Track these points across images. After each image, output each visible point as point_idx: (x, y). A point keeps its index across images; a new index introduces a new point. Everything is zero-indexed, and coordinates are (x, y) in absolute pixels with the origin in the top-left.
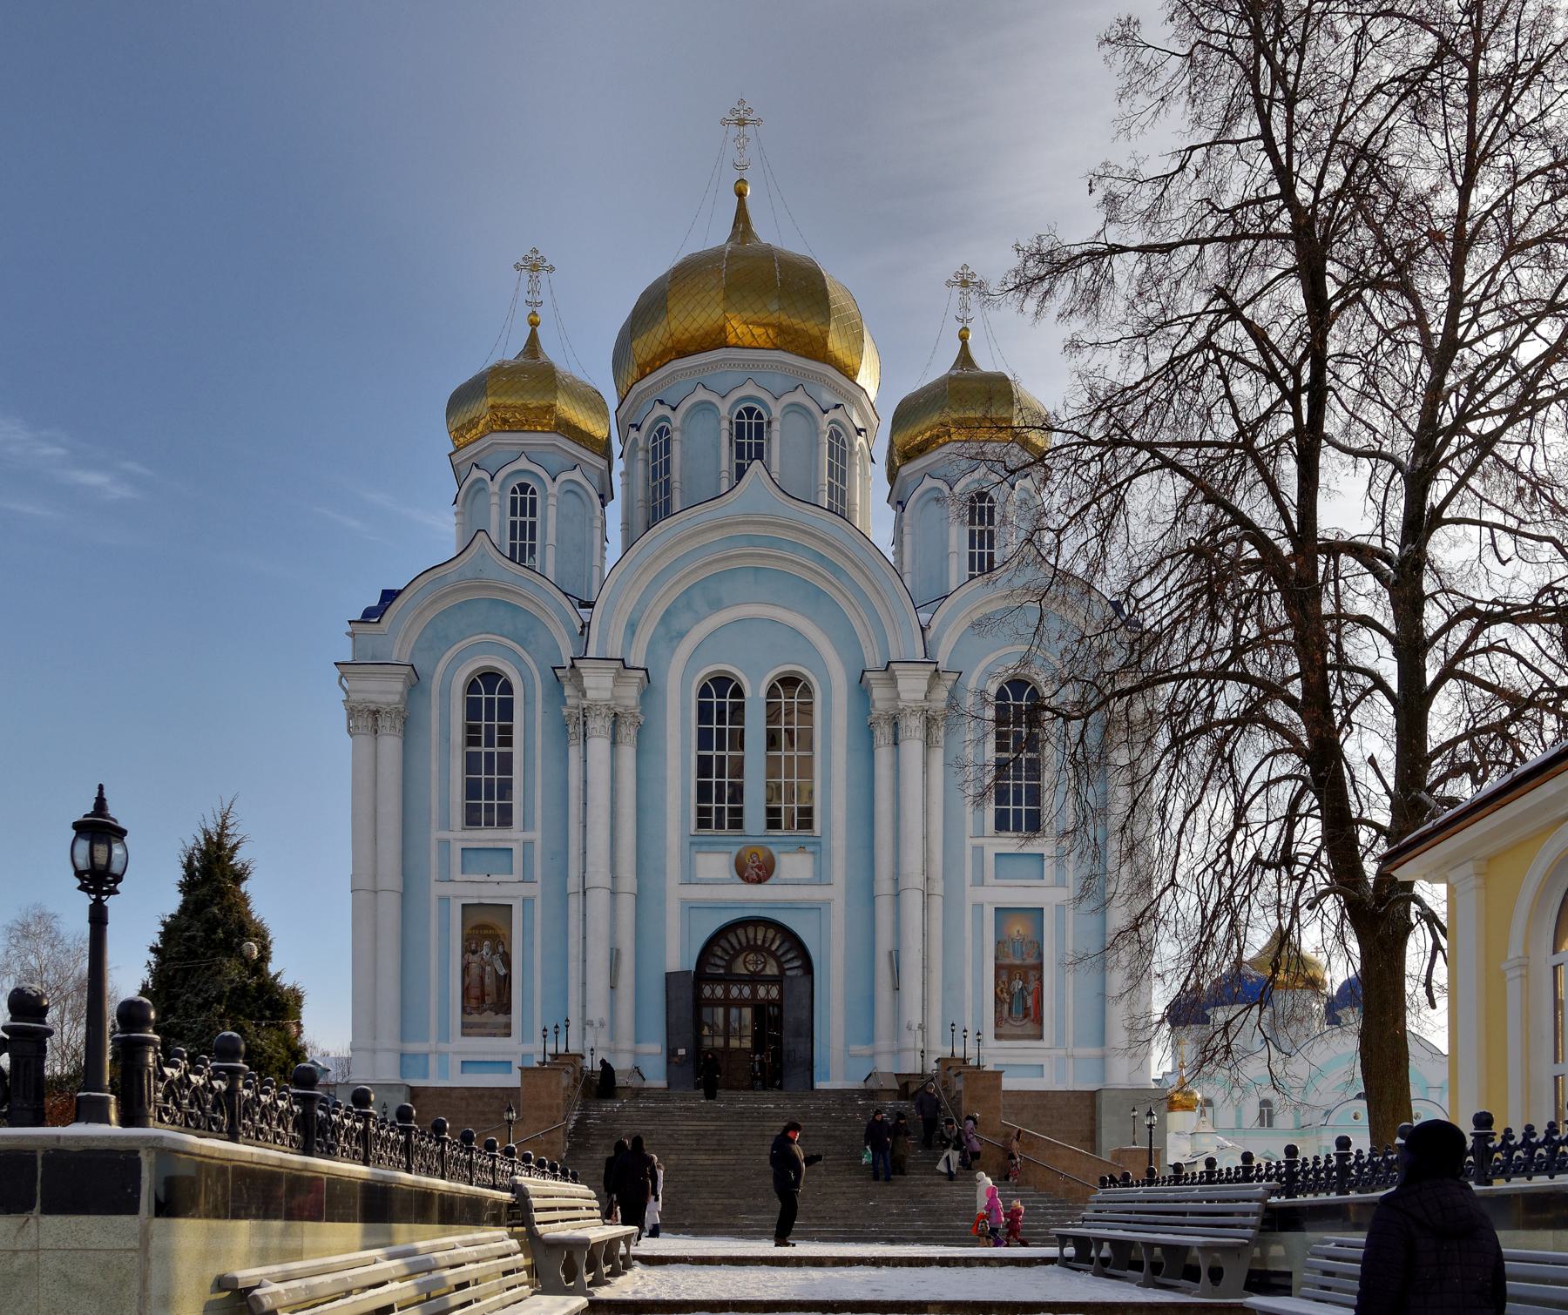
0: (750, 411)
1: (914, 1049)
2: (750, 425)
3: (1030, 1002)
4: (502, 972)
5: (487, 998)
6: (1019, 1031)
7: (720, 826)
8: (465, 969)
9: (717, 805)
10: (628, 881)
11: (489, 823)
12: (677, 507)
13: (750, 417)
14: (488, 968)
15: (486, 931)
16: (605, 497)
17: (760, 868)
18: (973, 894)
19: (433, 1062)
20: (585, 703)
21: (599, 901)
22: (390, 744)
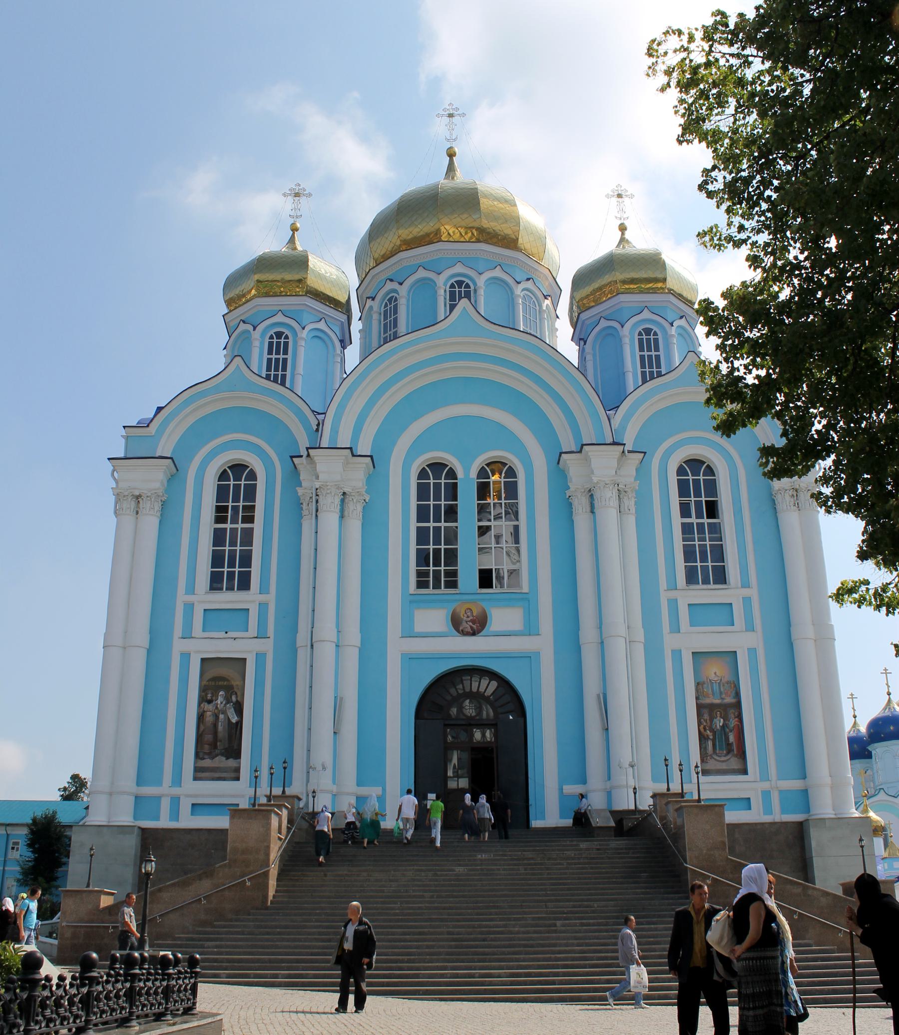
0: (460, 283)
1: (633, 783)
3: (732, 738)
4: (234, 719)
5: (219, 745)
6: (724, 766)
7: (437, 586)
8: (201, 717)
9: (435, 567)
10: (353, 636)
11: (230, 588)
12: (402, 328)
13: (460, 287)
14: (221, 716)
15: (221, 682)
16: (345, 342)
17: (473, 621)
18: (670, 642)
19: (165, 804)
20: (317, 485)
21: (326, 652)
22: (150, 522)
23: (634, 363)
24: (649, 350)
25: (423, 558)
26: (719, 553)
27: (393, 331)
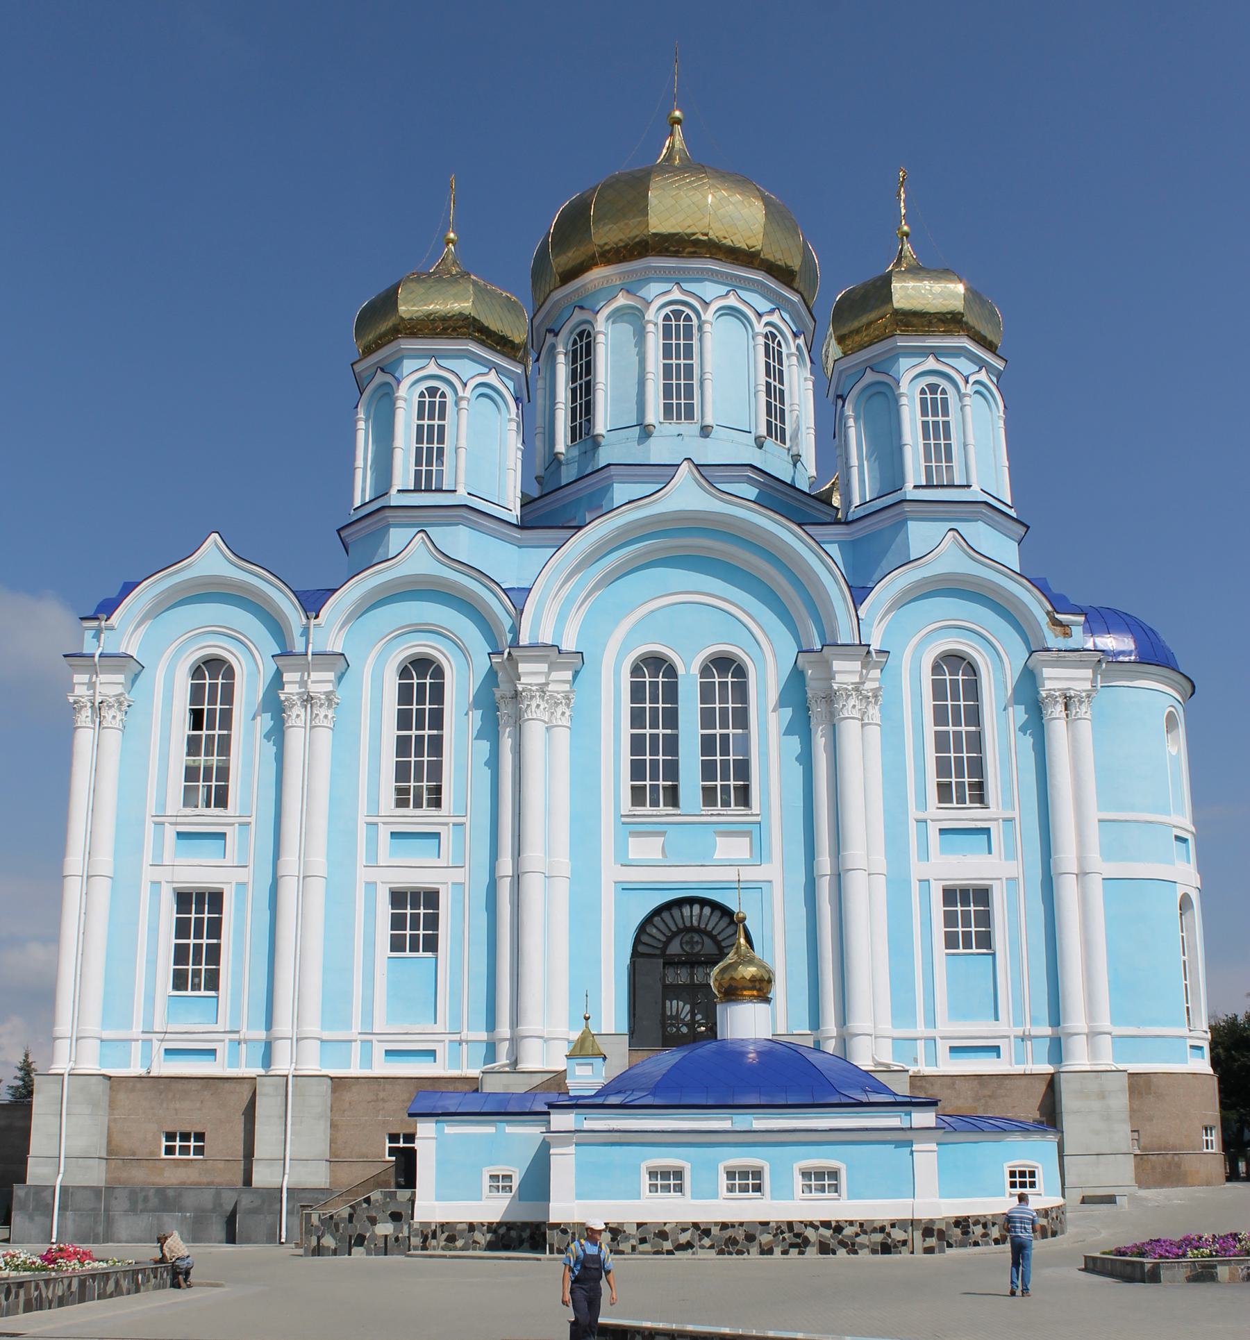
0: (678, 314)
2: (678, 326)
9: (653, 780)
13: (678, 319)
18: (917, 869)
23: (914, 431)
24: (935, 414)
25: (637, 770)
26: (978, 766)
27: (584, 379)
